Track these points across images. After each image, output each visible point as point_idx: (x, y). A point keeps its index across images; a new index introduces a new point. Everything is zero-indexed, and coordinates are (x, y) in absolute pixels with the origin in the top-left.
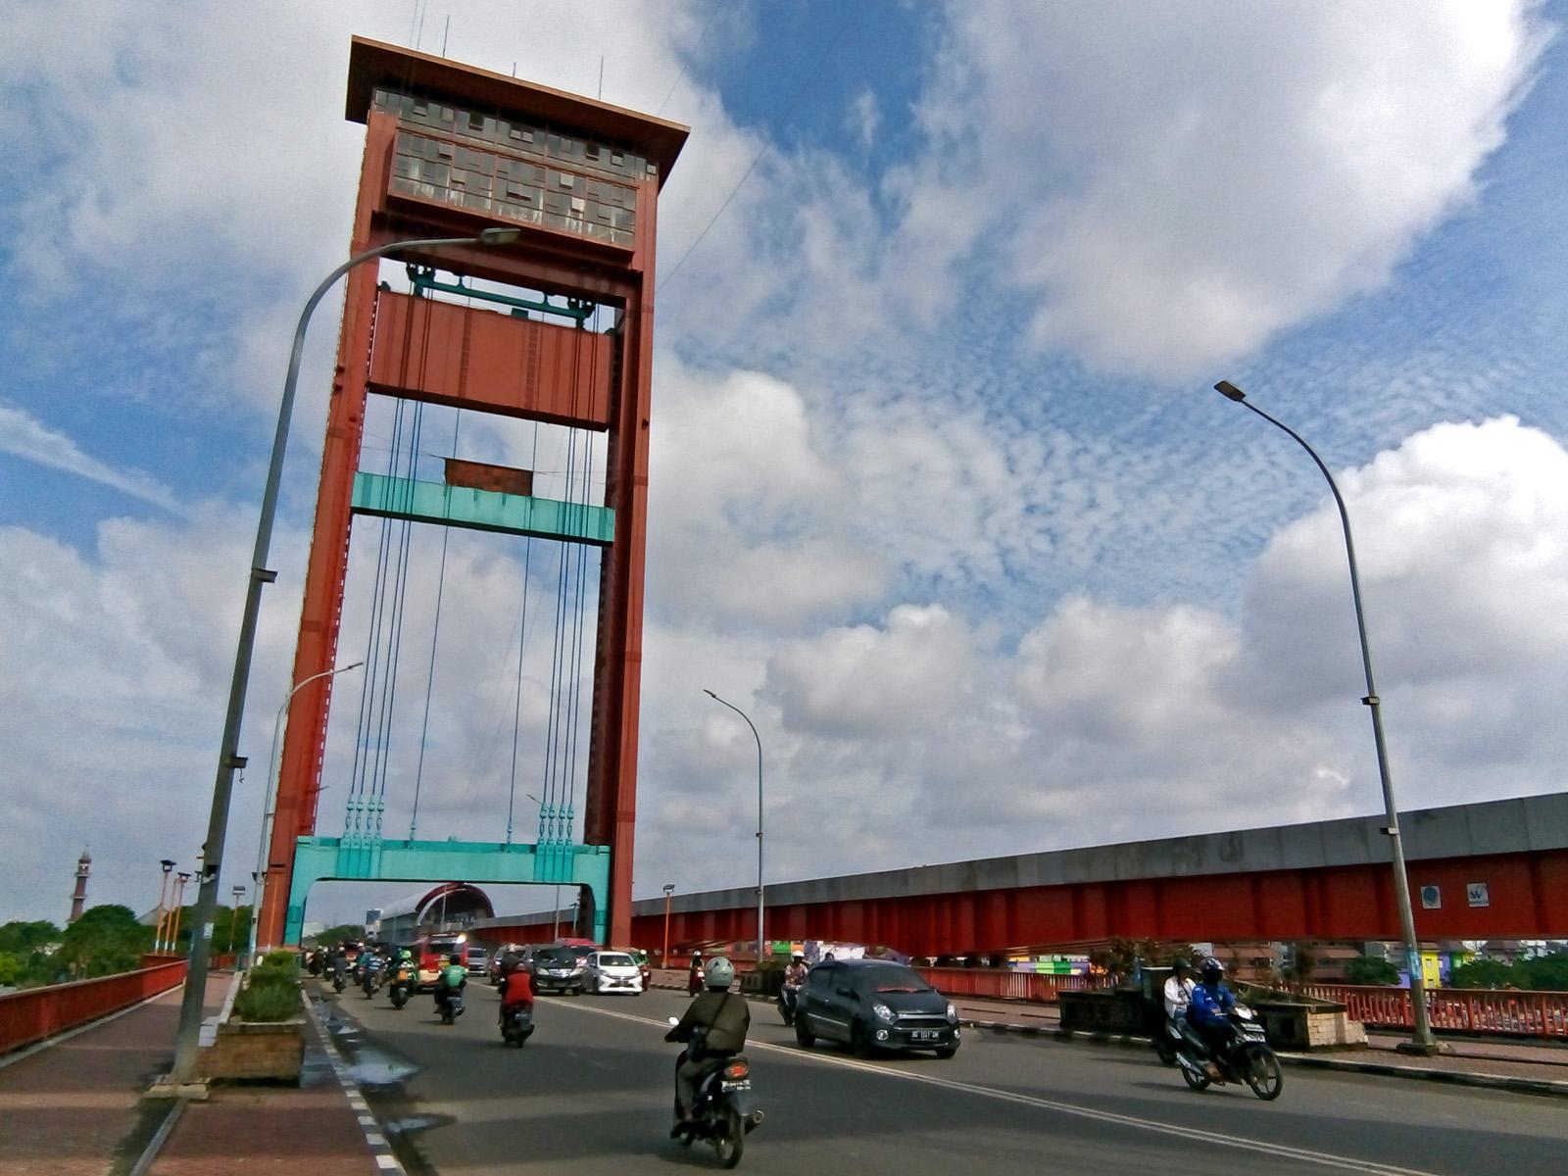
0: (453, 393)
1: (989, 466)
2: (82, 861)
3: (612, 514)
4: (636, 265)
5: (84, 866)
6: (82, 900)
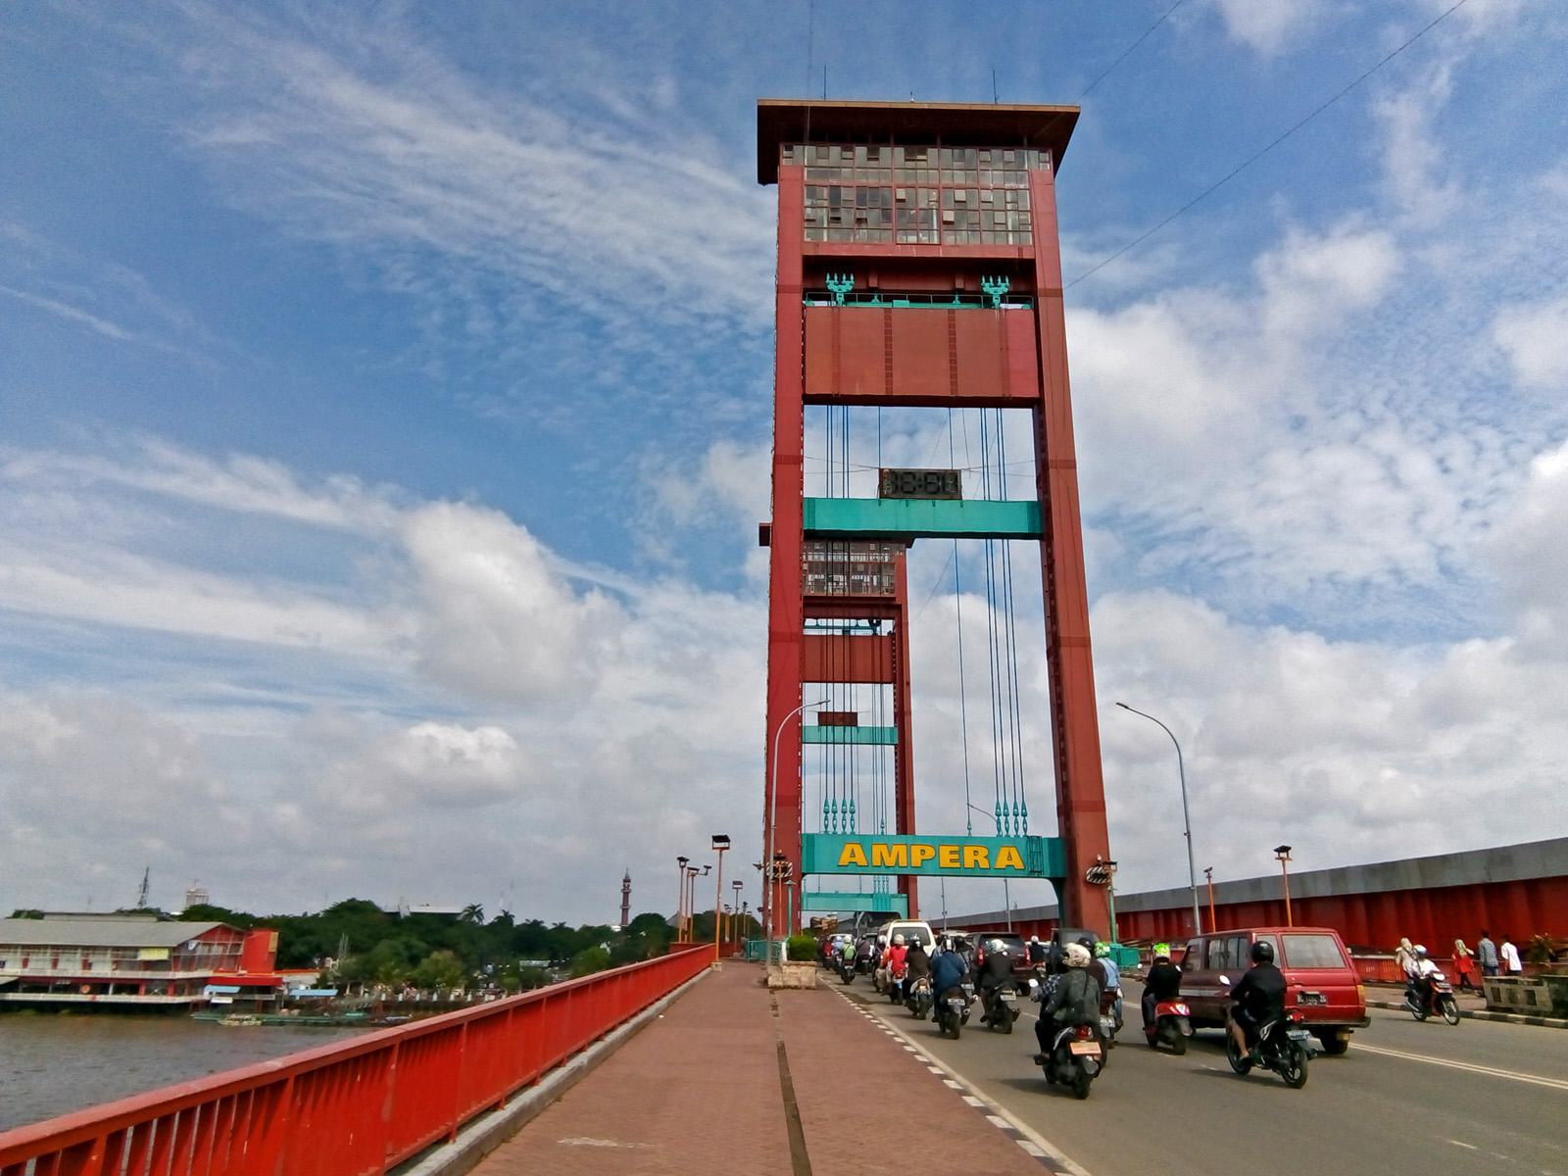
0: (880, 391)
1: (1418, 466)
2: (625, 881)
3: (896, 730)
4: (898, 602)
5: (627, 884)
6: (627, 909)
